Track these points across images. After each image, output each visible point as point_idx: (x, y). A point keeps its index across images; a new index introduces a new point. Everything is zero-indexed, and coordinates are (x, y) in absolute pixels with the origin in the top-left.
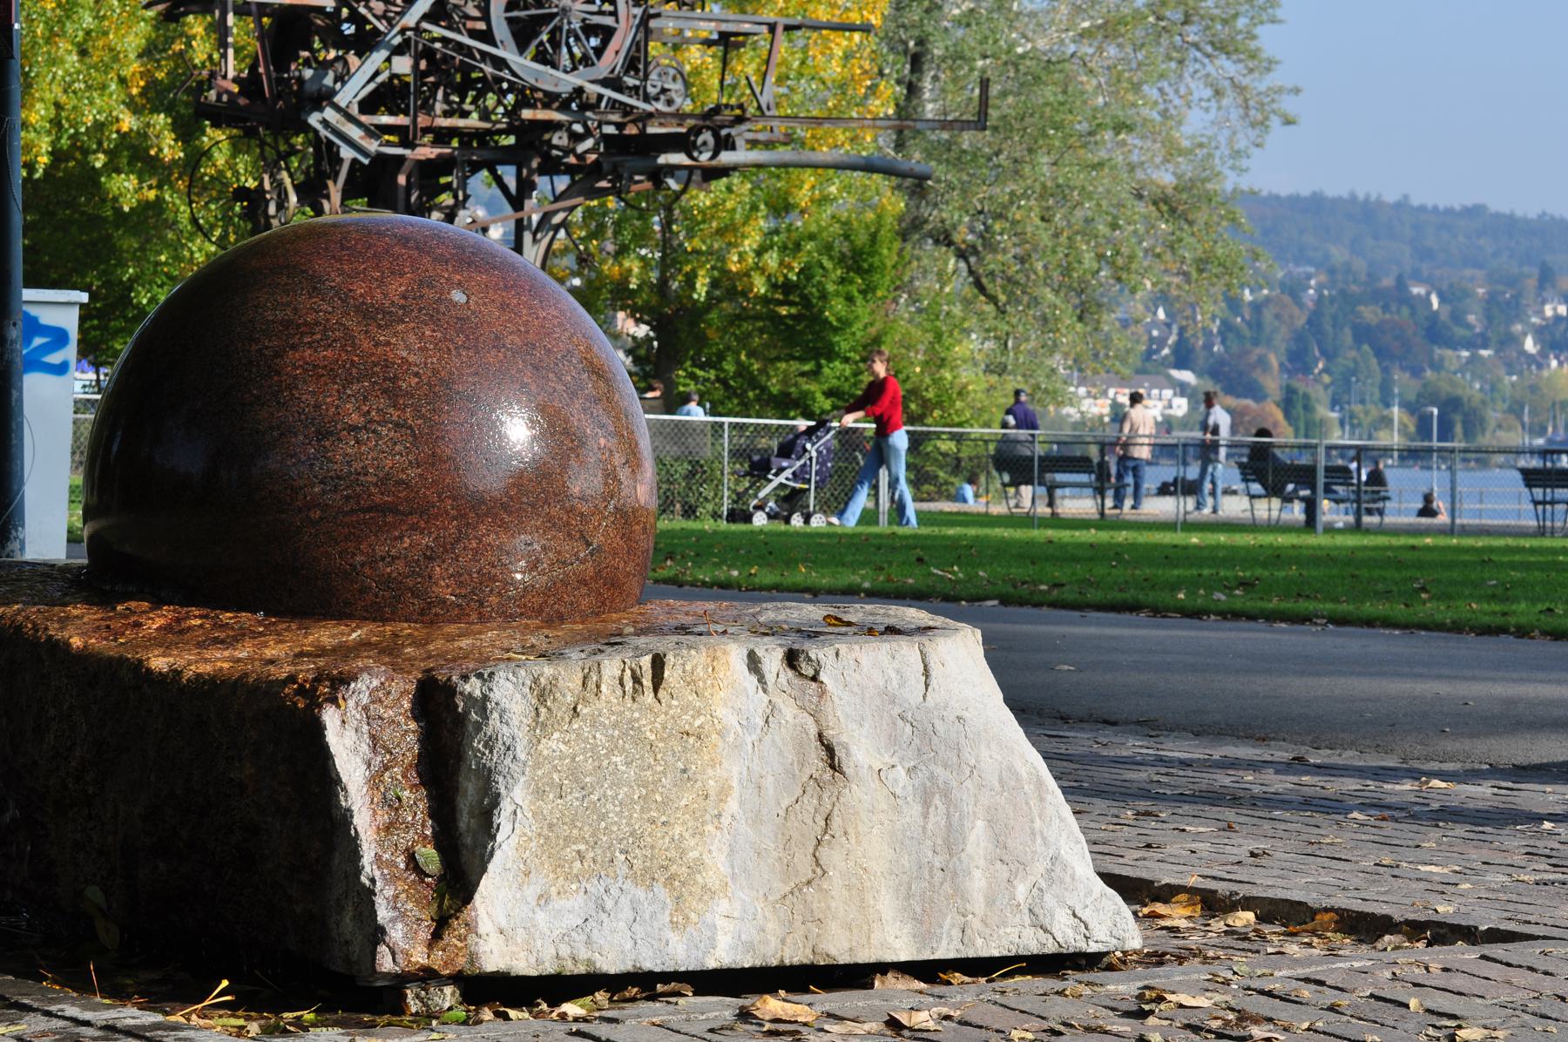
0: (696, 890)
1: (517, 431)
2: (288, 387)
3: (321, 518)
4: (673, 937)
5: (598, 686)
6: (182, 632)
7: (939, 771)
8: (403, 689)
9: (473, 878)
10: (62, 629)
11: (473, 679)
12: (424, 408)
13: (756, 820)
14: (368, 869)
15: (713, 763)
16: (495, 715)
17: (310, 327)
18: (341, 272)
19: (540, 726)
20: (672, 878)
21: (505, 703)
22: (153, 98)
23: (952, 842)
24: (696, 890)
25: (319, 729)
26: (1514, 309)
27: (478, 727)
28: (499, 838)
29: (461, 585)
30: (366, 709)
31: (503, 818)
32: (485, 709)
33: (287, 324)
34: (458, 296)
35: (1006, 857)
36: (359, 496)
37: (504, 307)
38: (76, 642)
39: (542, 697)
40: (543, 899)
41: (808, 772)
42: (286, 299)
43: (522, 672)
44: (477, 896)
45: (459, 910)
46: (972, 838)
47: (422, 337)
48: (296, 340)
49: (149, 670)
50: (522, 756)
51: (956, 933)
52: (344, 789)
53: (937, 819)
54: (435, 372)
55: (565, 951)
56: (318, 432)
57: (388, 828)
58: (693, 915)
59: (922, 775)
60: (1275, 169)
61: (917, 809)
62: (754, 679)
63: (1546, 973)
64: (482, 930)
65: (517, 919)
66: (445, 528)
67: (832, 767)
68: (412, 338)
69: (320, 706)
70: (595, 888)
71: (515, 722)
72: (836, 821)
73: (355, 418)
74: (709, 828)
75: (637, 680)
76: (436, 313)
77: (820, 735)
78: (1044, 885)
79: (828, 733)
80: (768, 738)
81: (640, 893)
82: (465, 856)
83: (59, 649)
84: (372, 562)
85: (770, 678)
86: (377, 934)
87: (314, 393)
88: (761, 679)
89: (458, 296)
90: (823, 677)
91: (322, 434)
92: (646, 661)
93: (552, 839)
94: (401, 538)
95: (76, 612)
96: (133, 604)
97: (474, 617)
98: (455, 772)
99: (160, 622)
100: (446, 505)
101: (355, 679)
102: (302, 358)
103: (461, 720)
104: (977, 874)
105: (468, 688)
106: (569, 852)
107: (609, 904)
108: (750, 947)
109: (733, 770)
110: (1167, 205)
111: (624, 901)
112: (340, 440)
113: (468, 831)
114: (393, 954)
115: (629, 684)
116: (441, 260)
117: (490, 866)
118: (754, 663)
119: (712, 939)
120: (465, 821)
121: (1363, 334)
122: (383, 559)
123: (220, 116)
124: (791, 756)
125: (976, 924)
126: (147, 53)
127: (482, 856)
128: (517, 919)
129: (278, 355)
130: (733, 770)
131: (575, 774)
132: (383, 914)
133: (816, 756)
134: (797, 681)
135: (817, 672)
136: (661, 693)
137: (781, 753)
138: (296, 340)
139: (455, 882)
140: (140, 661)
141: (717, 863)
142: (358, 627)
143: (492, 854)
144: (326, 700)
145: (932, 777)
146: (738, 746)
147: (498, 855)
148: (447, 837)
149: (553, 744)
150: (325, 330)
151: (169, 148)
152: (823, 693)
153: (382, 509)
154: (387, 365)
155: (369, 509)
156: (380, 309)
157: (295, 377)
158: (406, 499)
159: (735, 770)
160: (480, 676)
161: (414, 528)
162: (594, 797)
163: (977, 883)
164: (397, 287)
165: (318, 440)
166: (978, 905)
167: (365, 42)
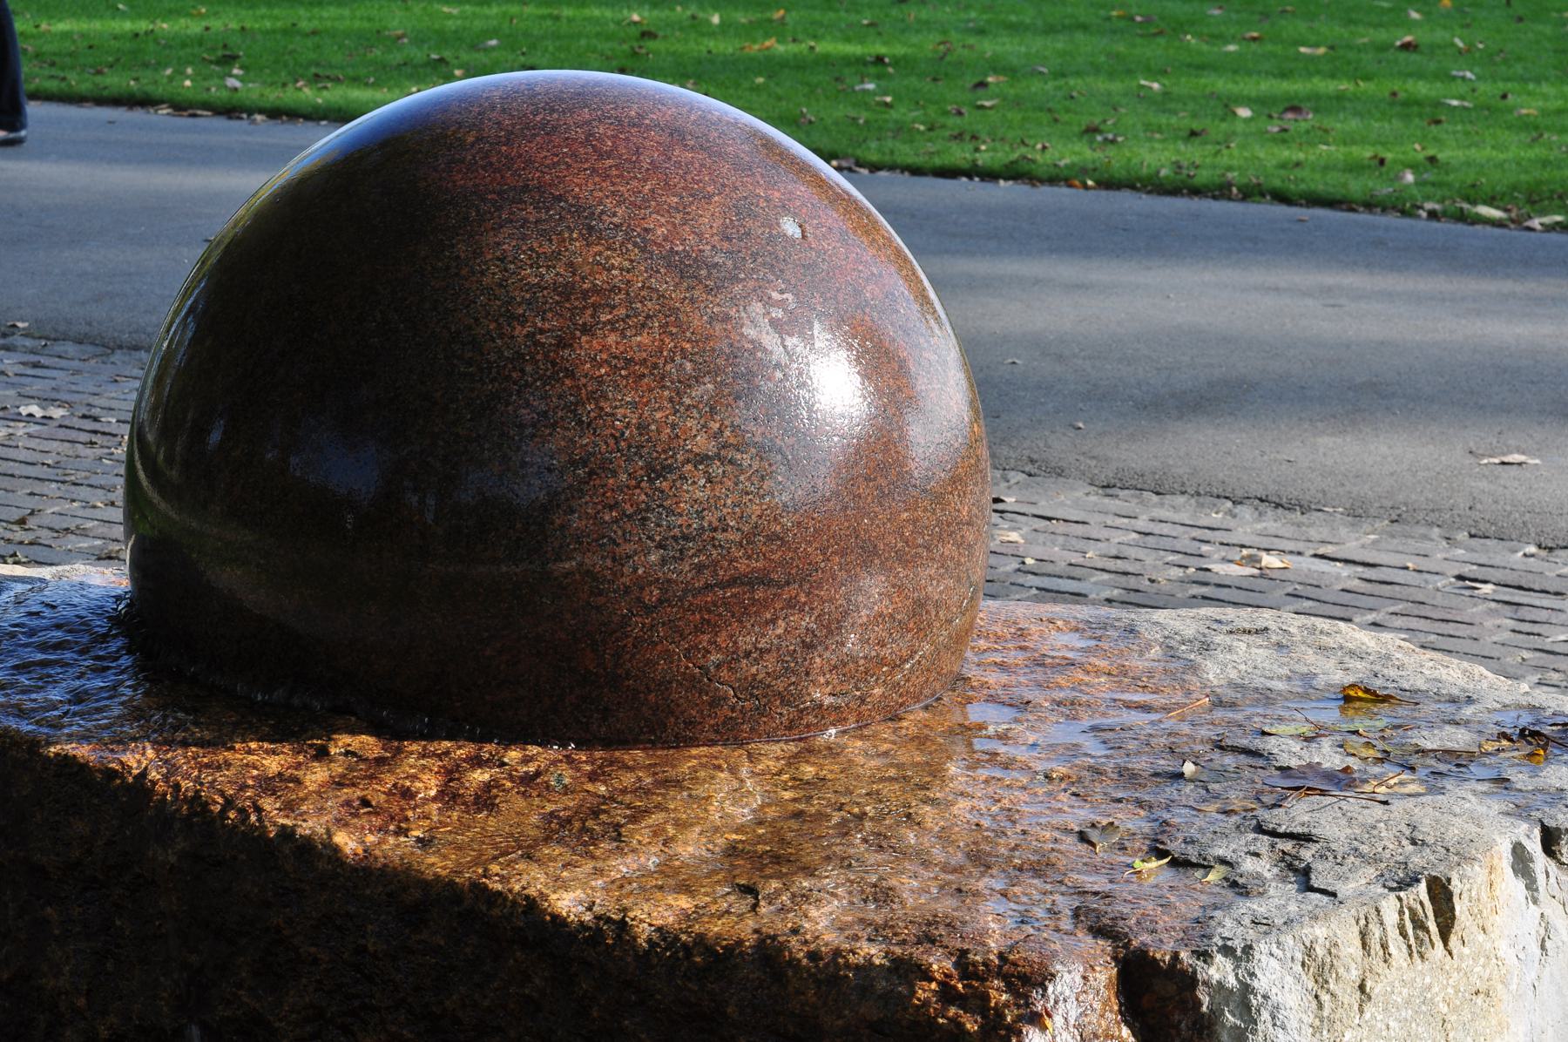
2: (591, 397)
3: (660, 602)
5: (1384, 947)
8: (1105, 975)
11: (1219, 958)
16: (1265, 1015)
21: (1277, 996)
33: (566, 291)
36: (715, 563)
38: (347, 842)
39: (1321, 979)
42: (547, 248)
43: (1288, 940)
48: (587, 317)
56: (650, 468)
62: (1519, 886)
66: (831, 600)
71: (1292, 1024)
73: (702, 444)
75: (1419, 925)
80: (1546, 973)
87: (635, 405)
88: (1531, 886)
91: (657, 471)
94: (774, 621)
102: (605, 348)
112: (683, 478)
122: (748, 654)
129: (562, 343)
136: (1454, 941)
138: (587, 317)
150: (630, 302)
153: (749, 581)
155: (733, 582)
157: (600, 380)
158: (782, 563)
160: (1227, 951)
161: (791, 604)
165: (651, 480)
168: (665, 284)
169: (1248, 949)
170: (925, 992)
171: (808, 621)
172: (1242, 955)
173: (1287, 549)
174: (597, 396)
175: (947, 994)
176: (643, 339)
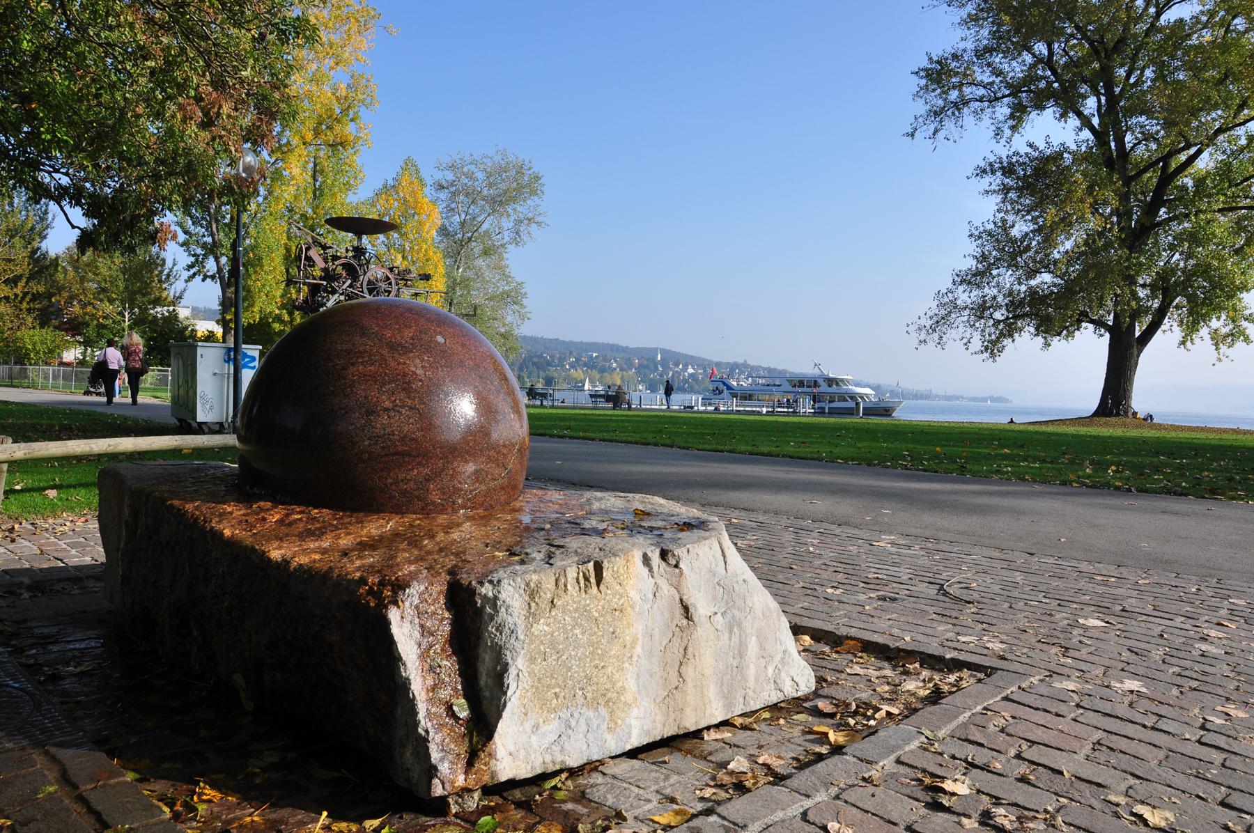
0: (621, 705)
1: (464, 407)
4: (608, 736)
6: (290, 524)
7: (736, 612)
8: (439, 588)
9: (492, 721)
10: (220, 521)
12: (422, 399)
13: (650, 655)
14: (423, 723)
15: (629, 626)
16: (503, 609)
17: (362, 354)
18: (378, 325)
19: (532, 616)
20: (608, 701)
22: (283, 306)
23: (741, 654)
24: (621, 705)
25: (386, 624)
26: (564, 359)
27: (492, 618)
28: (509, 693)
29: (444, 493)
30: (417, 607)
31: (510, 680)
32: (495, 605)
33: (349, 352)
34: (440, 339)
35: (765, 655)
37: (463, 345)
38: (227, 532)
40: (536, 727)
41: (675, 622)
44: (496, 735)
45: (484, 745)
46: (750, 647)
47: (423, 360)
49: (269, 559)
50: (522, 637)
51: (741, 700)
52: (404, 664)
53: (735, 640)
54: (430, 379)
55: (548, 758)
56: (367, 411)
57: (434, 688)
58: (619, 722)
59: (729, 616)
60: (526, 329)
61: (726, 635)
62: (646, 570)
63: (1058, 715)
64: (499, 756)
65: (516, 750)
67: (687, 618)
68: (418, 361)
69: (386, 607)
70: (564, 714)
71: (516, 614)
72: (690, 650)
74: (626, 665)
75: (587, 579)
76: (430, 348)
77: (681, 600)
78: (780, 666)
79: (685, 598)
81: (591, 714)
82: (485, 704)
83: (218, 535)
84: (396, 483)
85: (655, 569)
86: (432, 771)
88: (651, 570)
89: (440, 339)
90: (681, 565)
91: (369, 413)
92: (591, 565)
93: (539, 688)
95: (229, 509)
96: (262, 503)
97: (450, 510)
98: (477, 646)
99: (277, 517)
100: (430, 451)
101: (409, 586)
103: (479, 612)
104: (752, 666)
105: (483, 591)
106: (550, 694)
107: (573, 723)
108: (648, 733)
109: (638, 628)
110: (503, 336)
111: (582, 720)
113: (486, 686)
114: (443, 784)
115: (582, 581)
116: (428, 320)
117: (505, 714)
118: (646, 560)
119: (629, 733)
120: (484, 680)
121: (534, 364)
123: (298, 308)
124: (667, 615)
125: (751, 693)
126: (282, 296)
127: (498, 706)
128: (516, 750)
129: (343, 368)
130: (638, 628)
131: (553, 644)
132: (435, 755)
133: (679, 610)
134: (668, 569)
135: (678, 563)
136: (602, 587)
137: (662, 614)
139: (481, 727)
140: (264, 552)
141: (631, 685)
142: (390, 520)
143: (505, 706)
144: (390, 602)
145: (733, 617)
146: (640, 614)
147: (509, 705)
148: (471, 691)
149: (541, 627)
151: (286, 318)
152: (681, 573)
153: (403, 454)
154: (405, 375)
155: (396, 454)
156: (400, 345)
159: (640, 628)
160: (491, 582)
161: (419, 464)
162: (564, 657)
163: (752, 671)
164: (408, 334)
166: (751, 683)
167: (334, 292)
168: (385, 352)
169: (499, 581)
170: (363, 590)
171: (427, 471)
172: (496, 584)
173: (1041, 713)
174: (352, 386)
175: (370, 592)
176: (372, 368)
